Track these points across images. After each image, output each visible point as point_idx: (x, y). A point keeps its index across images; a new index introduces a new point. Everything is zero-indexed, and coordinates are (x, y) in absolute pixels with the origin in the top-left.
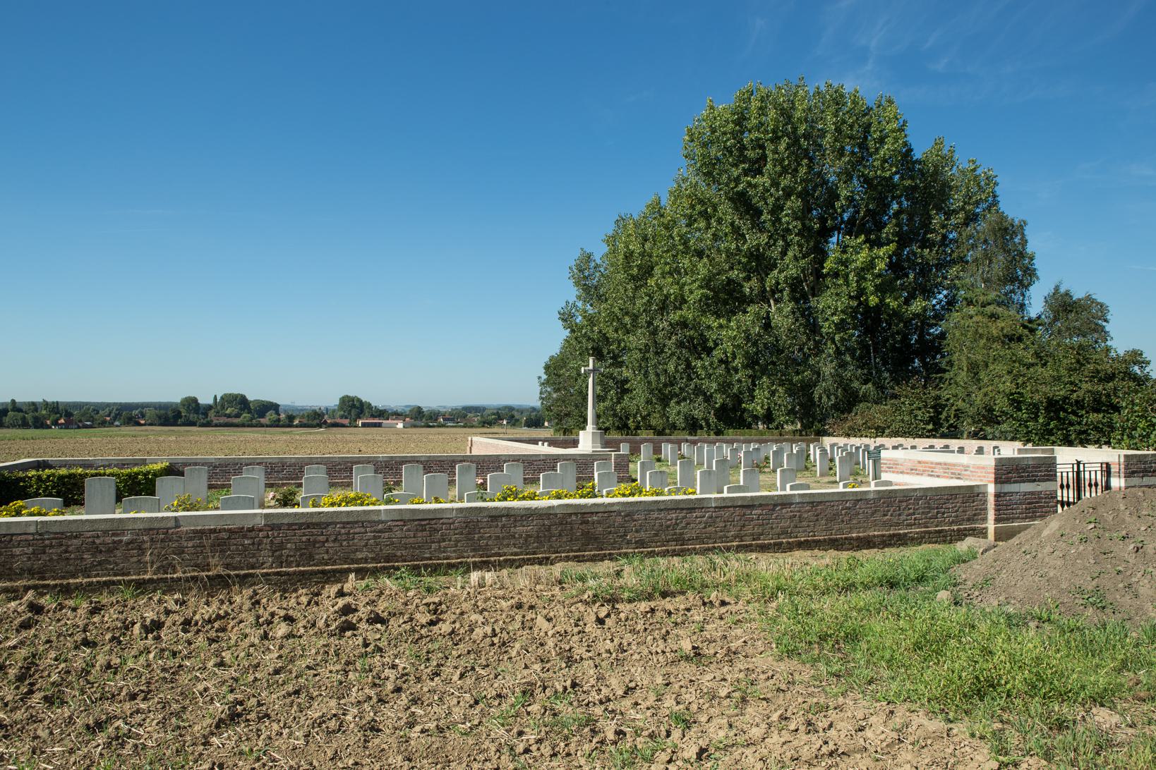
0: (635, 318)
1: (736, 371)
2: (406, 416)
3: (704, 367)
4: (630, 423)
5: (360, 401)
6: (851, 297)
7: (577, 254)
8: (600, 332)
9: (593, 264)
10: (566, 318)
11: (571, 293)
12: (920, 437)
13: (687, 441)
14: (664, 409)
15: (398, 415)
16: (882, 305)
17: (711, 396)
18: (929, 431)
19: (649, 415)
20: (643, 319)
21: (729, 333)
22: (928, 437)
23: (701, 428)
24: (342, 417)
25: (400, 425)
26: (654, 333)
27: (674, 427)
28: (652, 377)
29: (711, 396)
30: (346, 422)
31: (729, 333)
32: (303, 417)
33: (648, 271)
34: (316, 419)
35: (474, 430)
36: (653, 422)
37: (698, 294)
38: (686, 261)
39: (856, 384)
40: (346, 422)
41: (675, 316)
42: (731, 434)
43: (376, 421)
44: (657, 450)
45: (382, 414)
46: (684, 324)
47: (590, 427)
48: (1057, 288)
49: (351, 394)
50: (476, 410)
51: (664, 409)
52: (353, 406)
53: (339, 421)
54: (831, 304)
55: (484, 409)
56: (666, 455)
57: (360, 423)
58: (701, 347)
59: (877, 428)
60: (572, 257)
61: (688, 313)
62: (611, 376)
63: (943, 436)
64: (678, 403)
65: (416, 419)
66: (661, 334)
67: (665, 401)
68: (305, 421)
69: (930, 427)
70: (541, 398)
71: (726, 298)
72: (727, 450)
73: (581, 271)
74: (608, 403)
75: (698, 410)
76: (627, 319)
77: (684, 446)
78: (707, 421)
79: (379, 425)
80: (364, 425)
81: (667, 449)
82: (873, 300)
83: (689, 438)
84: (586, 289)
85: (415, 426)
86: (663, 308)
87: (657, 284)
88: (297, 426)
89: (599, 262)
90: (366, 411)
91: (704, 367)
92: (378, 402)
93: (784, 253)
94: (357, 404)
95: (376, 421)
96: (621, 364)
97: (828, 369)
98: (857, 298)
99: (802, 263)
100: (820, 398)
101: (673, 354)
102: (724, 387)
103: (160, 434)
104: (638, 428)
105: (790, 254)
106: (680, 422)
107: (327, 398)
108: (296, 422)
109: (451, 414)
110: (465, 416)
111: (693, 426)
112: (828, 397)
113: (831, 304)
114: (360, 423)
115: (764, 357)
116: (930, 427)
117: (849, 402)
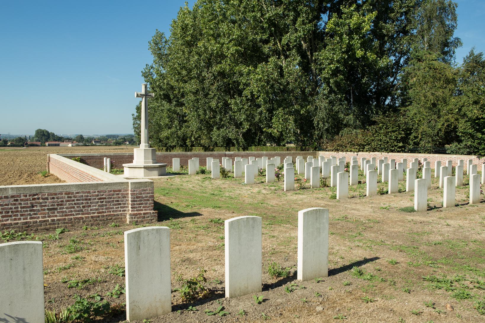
0: (190, 71)
1: (259, 106)
2: (74, 140)
3: (236, 103)
4: (188, 143)
5: (47, 132)
6: (343, 53)
7: (154, 33)
8: (168, 84)
9: (164, 40)
10: (146, 75)
11: (150, 59)
12: (392, 151)
13: (225, 155)
14: (209, 133)
15: (69, 140)
16: (364, 58)
17: (241, 124)
18: (400, 147)
19: (199, 137)
20: (194, 72)
21: (254, 78)
22: (398, 152)
23: (233, 145)
24: (37, 141)
25: (70, 145)
26: (202, 81)
27: (216, 144)
28: (201, 112)
29: (241, 124)
30: (39, 143)
31: (254, 78)
32: (13, 141)
33: (195, 39)
34: (21, 142)
35: (111, 147)
36: (202, 142)
37: (233, 50)
38: (226, 27)
39: (341, 116)
40: (39, 143)
41: (216, 68)
42: (253, 150)
43: (57, 143)
44: (203, 162)
45: (60, 139)
46: (222, 74)
47: (143, 145)
48: (472, 54)
49: (43, 128)
50: (114, 136)
51: (209, 133)
52: (44, 135)
53: (35, 143)
54: (329, 57)
55: (118, 136)
56: (210, 167)
57: (47, 144)
58: (233, 89)
59: (359, 145)
60: (150, 36)
61: (225, 66)
62: (175, 112)
63: (412, 151)
64: (218, 129)
65: (79, 142)
66: (207, 82)
67: (210, 128)
68: (14, 143)
69: (401, 144)
70: (134, 128)
71: (252, 55)
72: (264, 163)
73: (156, 44)
74: (173, 130)
75: (231, 133)
76: (184, 72)
77: (225, 160)
78: (237, 140)
79: (58, 145)
80: (49, 145)
81: (211, 163)
82: (359, 53)
83: (227, 153)
84: (160, 56)
85: (78, 146)
86: (209, 65)
87: (204, 46)
88: (9, 146)
89: (168, 39)
90: (51, 137)
91: (236, 103)
92: (59, 133)
93: (294, 21)
94: (46, 134)
95: (57, 143)
96: (182, 105)
97: (323, 104)
98: (346, 52)
99: (308, 26)
100: (318, 124)
101: (215, 95)
102: (250, 118)
103: (20, 150)
104: (193, 146)
105: (300, 20)
106: (220, 141)
107: (28, 131)
108: (9, 144)
109: (98, 139)
110: (106, 140)
111: (228, 143)
112: (323, 123)
113: (329, 57)
114: (47, 144)
115: (279, 96)
116: (401, 144)
117: (336, 126)
